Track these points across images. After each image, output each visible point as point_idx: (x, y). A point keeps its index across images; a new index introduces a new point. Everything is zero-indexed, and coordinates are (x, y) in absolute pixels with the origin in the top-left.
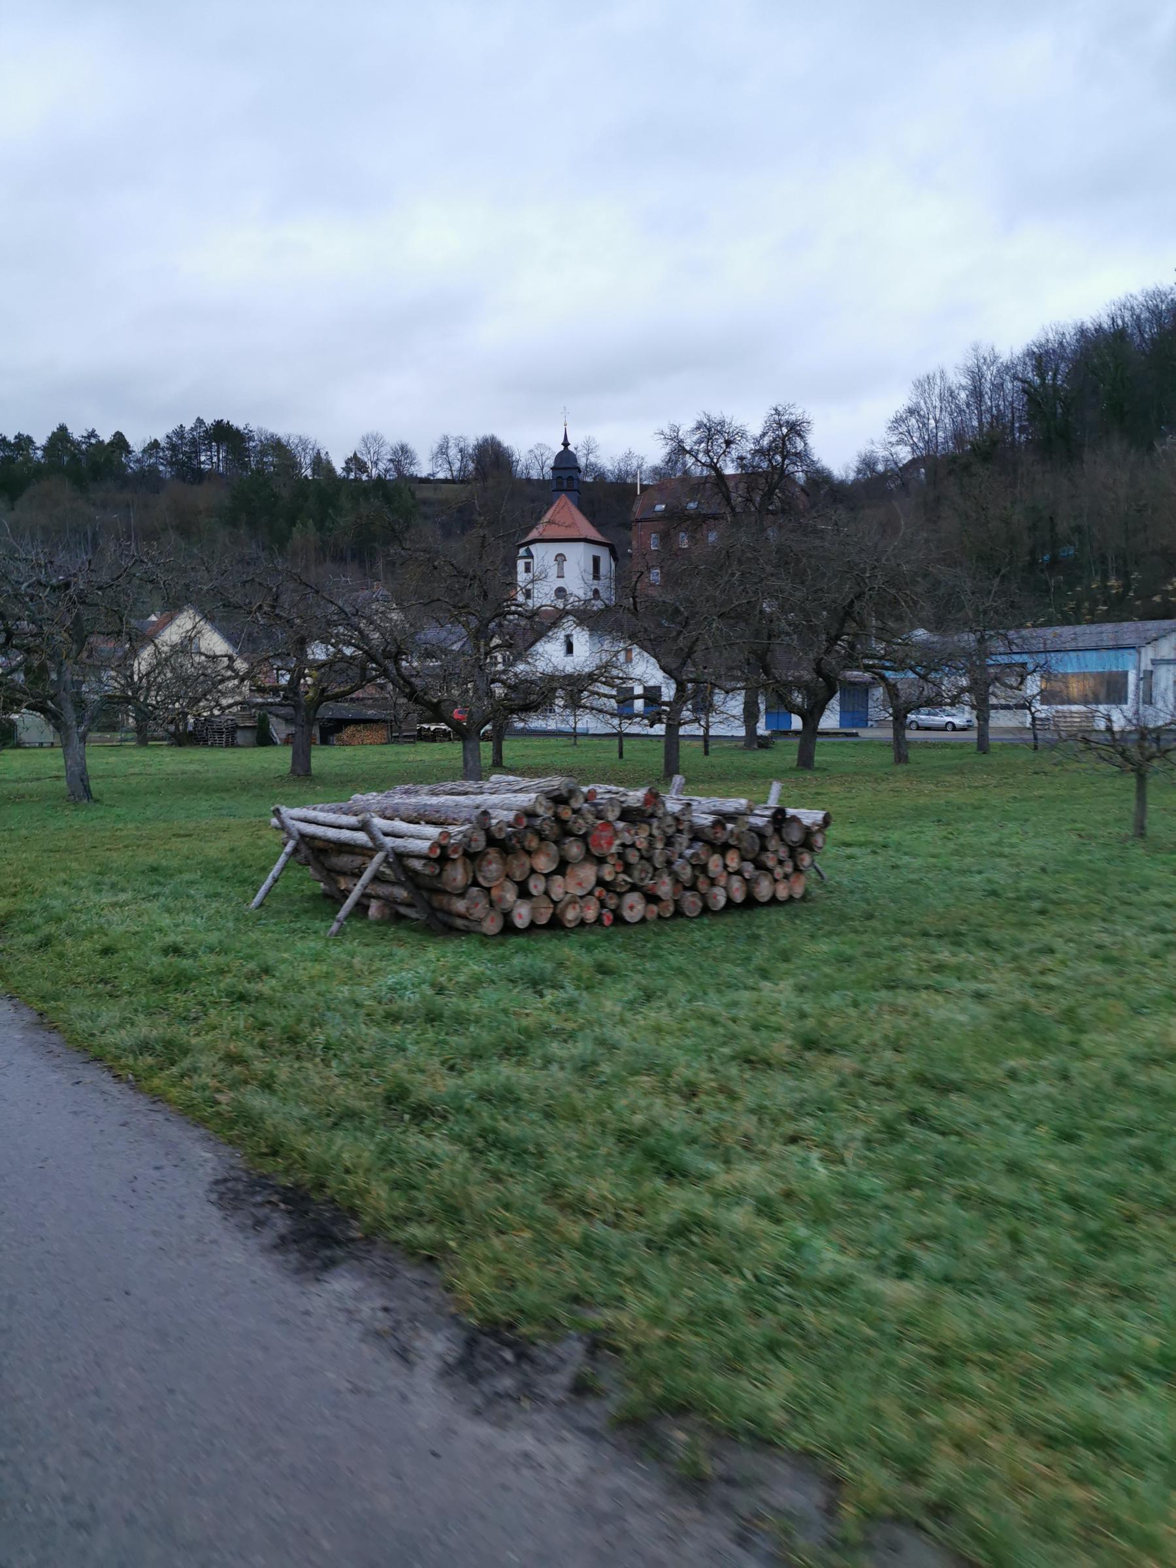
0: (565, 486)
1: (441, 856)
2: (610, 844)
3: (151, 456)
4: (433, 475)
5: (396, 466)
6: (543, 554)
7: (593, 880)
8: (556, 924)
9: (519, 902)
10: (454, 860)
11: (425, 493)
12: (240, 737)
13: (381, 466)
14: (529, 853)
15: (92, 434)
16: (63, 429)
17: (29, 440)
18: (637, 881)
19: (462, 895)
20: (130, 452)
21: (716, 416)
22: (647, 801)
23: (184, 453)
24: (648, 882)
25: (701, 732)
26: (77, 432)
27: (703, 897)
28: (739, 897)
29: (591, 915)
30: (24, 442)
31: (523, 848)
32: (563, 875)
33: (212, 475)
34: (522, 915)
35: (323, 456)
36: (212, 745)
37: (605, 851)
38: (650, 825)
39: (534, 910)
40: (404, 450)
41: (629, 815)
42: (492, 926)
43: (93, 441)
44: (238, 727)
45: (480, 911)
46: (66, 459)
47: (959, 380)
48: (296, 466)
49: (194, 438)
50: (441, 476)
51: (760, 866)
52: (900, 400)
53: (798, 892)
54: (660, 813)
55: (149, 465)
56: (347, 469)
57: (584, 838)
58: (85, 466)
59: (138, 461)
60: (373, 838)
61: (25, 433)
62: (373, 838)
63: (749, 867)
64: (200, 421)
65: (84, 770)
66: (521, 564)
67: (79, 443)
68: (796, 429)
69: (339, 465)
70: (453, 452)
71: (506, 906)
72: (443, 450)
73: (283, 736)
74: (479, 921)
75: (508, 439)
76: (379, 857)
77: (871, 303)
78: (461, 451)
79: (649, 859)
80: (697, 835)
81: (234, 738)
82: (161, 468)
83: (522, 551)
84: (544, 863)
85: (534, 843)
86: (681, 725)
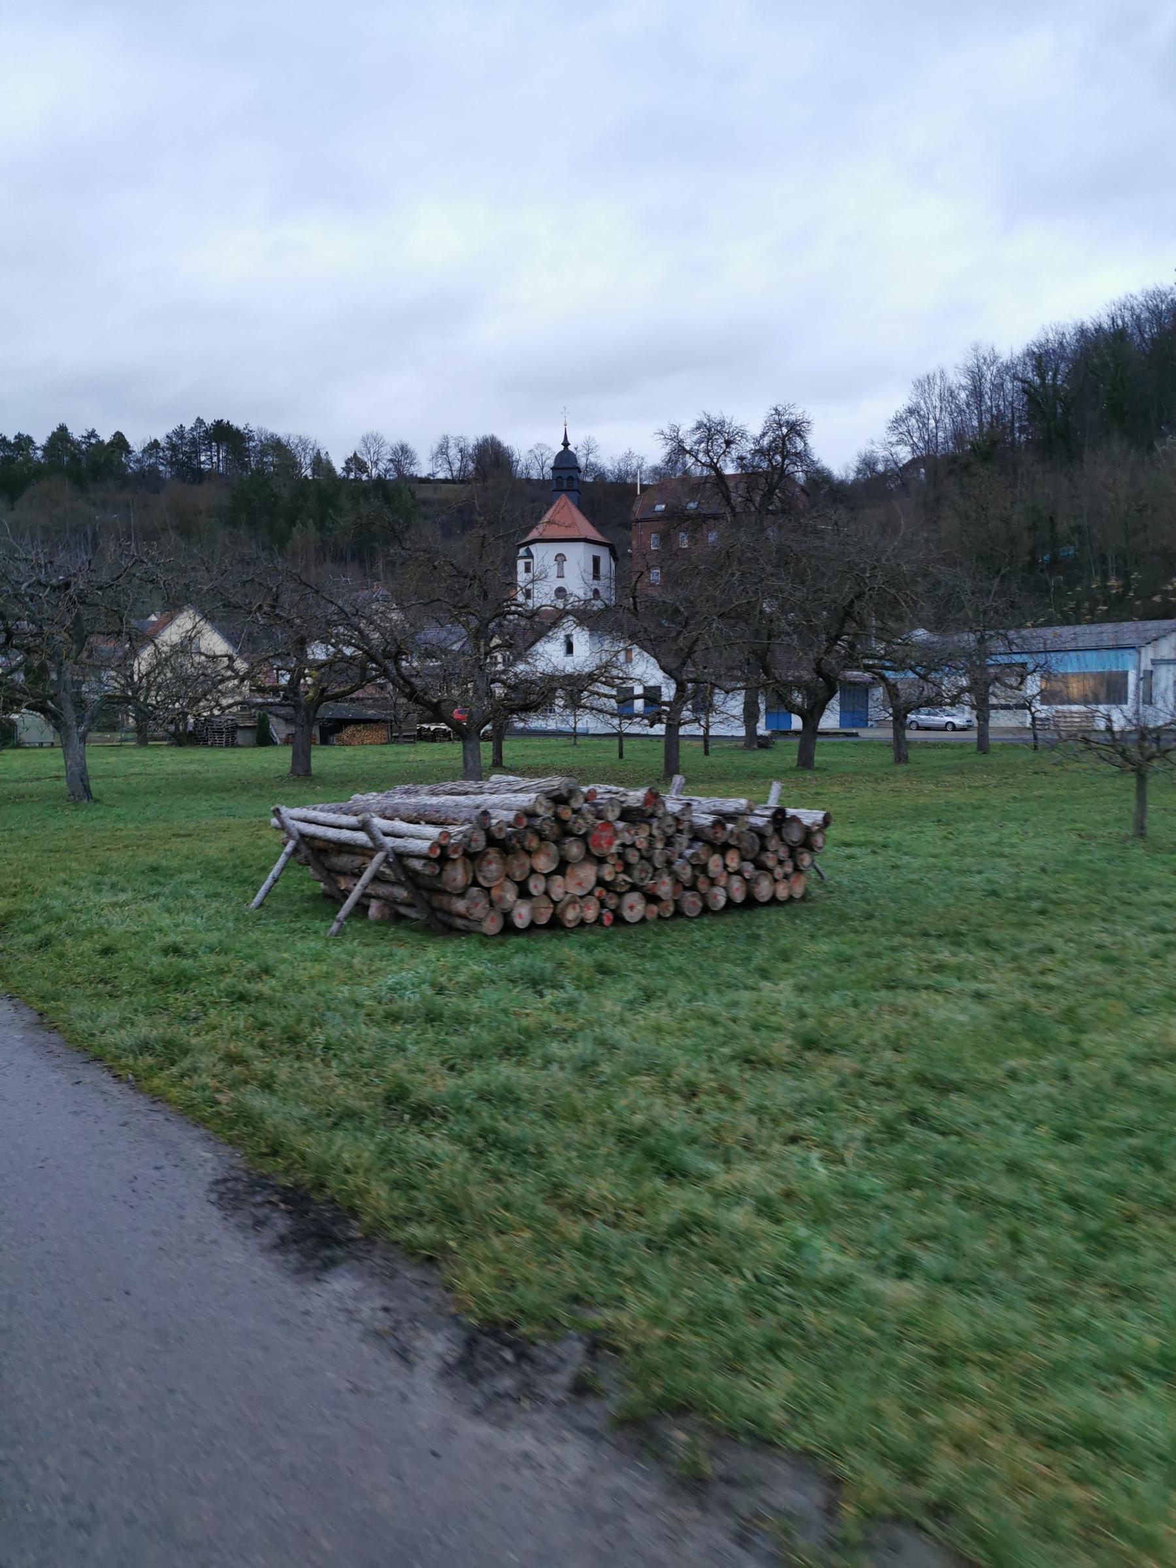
0: (565, 486)
1: (441, 856)
2: (610, 844)
3: (151, 456)
4: (433, 475)
5: (396, 466)
6: (543, 554)
7: (593, 880)
8: (556, 924)
9: (519, 902)
10: (454, 860)
11: (425, 493)
12: (240, 737)
13: (381, 466)
14: (529, 853)
15: (92, 434)
16: (63, 429)
17: (29, 440)
18: (637, 881)
19: (462, 895)
20: (130, 452)
21: (716, 416)
22: (647, 801)
23: (184, 453)
24: (648, 882)
25: (701, 732)
26: (77, 432)
27: (703, 897)
28: (739, 897)
29: (591, 915)
30: (24, 442)
31: (523, 848)
32: (563, 875)
33: (212, 475)
34: (522, 915)
35: (323, 456)
36: (212, 745)
37: (605, 851)
38: (650, 825)
39: (534, 910)
40: (404, 450)
41: (629, 815)
42: (492, 926)
43: (93, 441)
44: (238, 727)
45: (480, 911)
46: (66, 459)
47: (959, 380)
48: (296, 466)
49: (194, 438)
50: (441, 476)
51: (760, 866)
52: (900, 400)
53: (798, 892)
54: (660, 813)
55: (149, 465)
56: (347, 469)
57: (584, 838)
58: (85, 466)
59: (138, 461)
60: (373, 838)
61: (25, 433)
62: (373, 838)
63: (749, 867)
64: (200, 421)
65: (84, 770)
66: (521, 564)
67: (79, 443)
68: (796, 429)
69: (339, 465)
70: (453, 452)
71: (506, 906)
72: (443, 450)
73: (283, 736)
74: (479, 921)
75: (508, 439)
76: (379, 857)
77: (871, 303)
78: (461, 451)
79: (649, 859)
80: (697, 835)
81: (234, 738)
82: (161, 468)
83: (522, 551)
84: (544, 863)
85: (534, 843)
86: (681, 725)
